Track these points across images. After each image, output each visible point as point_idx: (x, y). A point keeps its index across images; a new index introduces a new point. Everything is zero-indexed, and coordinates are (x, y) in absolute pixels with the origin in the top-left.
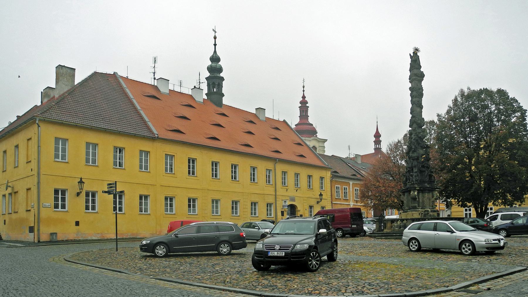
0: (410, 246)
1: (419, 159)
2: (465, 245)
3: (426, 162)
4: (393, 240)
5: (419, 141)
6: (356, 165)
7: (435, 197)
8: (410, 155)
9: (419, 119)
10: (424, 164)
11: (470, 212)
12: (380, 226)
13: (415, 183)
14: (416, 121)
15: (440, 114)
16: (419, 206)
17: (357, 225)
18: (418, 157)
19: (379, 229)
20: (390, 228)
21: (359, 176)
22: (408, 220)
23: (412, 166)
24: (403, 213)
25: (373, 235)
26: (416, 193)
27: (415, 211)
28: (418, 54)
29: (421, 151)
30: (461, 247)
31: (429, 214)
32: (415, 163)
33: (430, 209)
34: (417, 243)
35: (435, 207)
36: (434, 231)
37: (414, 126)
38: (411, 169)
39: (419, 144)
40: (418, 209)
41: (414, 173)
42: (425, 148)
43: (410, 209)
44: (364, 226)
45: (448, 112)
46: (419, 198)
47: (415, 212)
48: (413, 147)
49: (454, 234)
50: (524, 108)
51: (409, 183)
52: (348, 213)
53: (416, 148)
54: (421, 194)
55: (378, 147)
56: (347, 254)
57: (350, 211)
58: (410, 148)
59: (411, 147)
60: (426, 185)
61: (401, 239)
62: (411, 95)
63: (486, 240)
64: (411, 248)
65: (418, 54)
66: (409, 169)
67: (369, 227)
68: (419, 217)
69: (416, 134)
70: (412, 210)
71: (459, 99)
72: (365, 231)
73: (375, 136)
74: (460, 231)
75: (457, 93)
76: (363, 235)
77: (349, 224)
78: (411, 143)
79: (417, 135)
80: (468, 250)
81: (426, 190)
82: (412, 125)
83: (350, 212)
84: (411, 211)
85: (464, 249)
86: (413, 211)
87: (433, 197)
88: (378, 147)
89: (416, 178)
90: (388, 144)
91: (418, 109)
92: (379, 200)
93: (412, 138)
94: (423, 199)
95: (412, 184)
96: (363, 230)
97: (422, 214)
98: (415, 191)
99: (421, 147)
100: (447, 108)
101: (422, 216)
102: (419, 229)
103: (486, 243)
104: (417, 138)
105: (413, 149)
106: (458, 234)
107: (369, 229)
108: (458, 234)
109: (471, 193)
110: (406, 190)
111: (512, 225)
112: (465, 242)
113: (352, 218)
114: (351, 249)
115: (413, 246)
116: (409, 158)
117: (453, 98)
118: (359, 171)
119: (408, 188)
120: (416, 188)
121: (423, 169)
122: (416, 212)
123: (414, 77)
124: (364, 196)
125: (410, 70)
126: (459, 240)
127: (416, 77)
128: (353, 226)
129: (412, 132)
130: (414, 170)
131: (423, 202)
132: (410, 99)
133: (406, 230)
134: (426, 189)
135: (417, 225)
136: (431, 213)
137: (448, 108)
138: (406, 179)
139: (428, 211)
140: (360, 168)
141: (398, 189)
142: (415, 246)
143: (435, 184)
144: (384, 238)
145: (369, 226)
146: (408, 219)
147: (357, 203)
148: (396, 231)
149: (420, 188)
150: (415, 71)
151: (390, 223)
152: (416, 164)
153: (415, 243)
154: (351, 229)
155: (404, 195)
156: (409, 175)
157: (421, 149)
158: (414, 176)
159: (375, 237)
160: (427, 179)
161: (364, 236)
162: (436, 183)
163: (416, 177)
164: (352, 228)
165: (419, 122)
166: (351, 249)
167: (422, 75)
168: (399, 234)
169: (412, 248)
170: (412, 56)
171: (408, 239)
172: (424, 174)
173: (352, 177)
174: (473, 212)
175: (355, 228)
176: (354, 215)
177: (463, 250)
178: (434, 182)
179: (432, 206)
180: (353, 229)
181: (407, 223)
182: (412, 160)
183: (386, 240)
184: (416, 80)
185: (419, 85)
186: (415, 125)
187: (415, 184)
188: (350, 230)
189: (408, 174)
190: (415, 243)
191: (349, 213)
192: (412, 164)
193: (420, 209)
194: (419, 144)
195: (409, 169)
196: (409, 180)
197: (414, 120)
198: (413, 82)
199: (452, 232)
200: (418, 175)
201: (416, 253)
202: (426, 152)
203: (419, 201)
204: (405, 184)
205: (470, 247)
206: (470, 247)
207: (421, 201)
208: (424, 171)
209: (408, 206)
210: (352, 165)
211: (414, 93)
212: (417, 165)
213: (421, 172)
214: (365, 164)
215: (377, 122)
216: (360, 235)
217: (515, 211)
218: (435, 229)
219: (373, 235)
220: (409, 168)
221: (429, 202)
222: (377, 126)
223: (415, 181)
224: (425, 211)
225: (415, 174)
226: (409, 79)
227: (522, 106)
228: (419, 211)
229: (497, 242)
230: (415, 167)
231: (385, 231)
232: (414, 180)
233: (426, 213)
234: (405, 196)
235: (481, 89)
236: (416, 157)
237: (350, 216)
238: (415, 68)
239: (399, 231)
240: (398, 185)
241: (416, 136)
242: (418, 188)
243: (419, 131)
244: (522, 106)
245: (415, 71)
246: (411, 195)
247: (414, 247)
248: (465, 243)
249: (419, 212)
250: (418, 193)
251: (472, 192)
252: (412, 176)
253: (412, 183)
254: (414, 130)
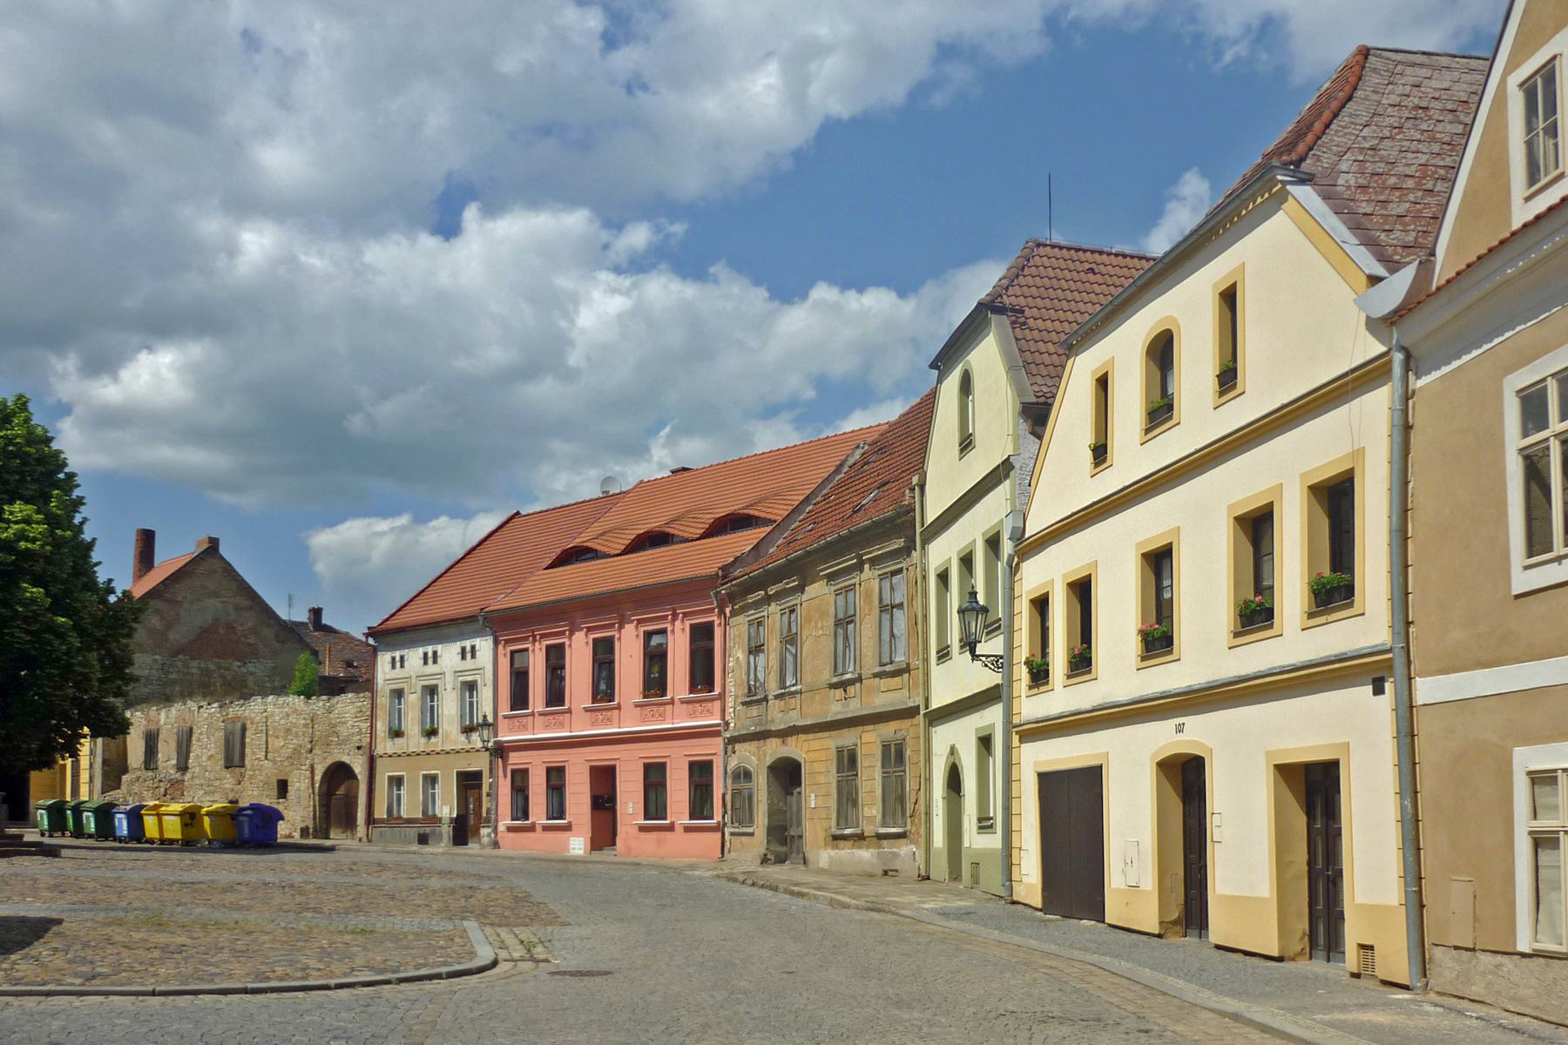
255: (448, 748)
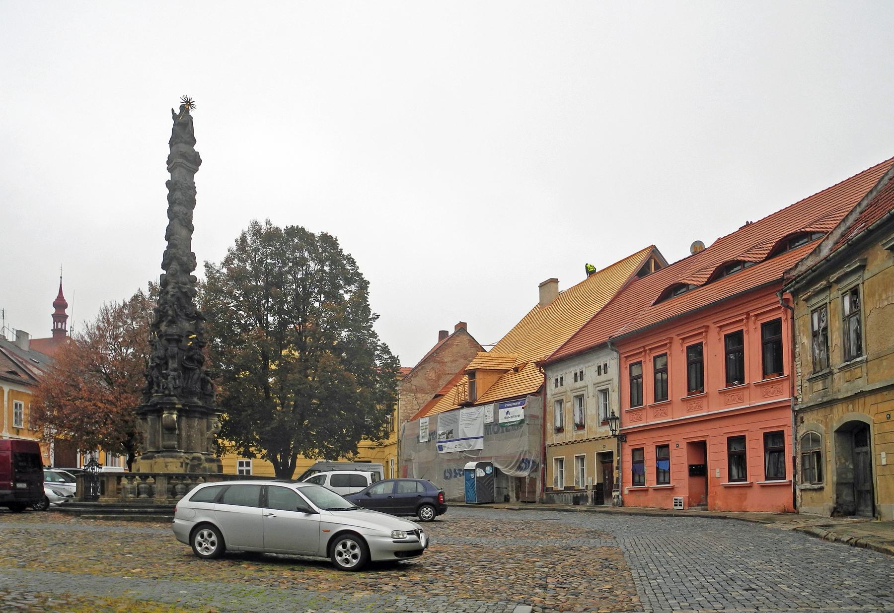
0: (196, 545)
1: (181, 341)
2: (344, 546)
3: (198, 351)
4: (125, 523)
5: (183, 301)
6: (17, 352)
7: (213, 429)
8: (161, 331)
9: (184, 252)
10: (192, 353)
11: (248, 468)
12: (87, 489)
13: (172, 393)
14: (178, 255)
15: (211, 262)
16: (179, 447)
17: (29, 483)
18: (179, 336)
19: (85, 495)
20: (116, 493)
21: (24, 377)
22: (157, 478)
23: (165, 356)
24: (142, 461)
25: (66, 508)
26: (175, 416)
27: (172, 457)
28: (191, 113)
29: (187, 325)
30: (331, 550)
31: (202, 467)
32: (173, 349)
33: (202, 454)
34: (214, 538)
35: (211, 452)
36: (260, 506)
37: (174, 266)
38: (163, 362)
39: (182, 307)
40: (178, 454)
41: (171, 371)
42: (193, 318)
43: (158, 452)
44: (45, 486)
45: (227, 262)
46: (180, 429)
47: (171, 460)
48: (170, 312)
49: (314, 517)
50: (366, 277)
51: (157, 392)
52: (7, 452)
53: (177, 315)
54: (184, 419)
55: (59, 327)
56: (24, 566)
57: (12, 448)
58: (161, 314)
59: (165, 311)
60: (196, 400)
61: (170, 520)
62: (169, 198)
63: (395, 533)
64: (199, 548)
65: (190, 111)
66: (158, 361)
67: (55, 490)
68: (181, 471)
69: (177, 286)
70: (164, 454)
71: (249, 239)
72: (46, 498)
73: (55, 305)
74: (327, 510)
75: (246, 226)
76: (42, 507)
77: (10, 480)
78: (166, 303)
79: (179, 288)
80: (350, 558)
81: (195, 411)
82: (169, 264)
83: (12, 451)
84: (163, 457)
85: (340, 554)
86: (167, 457)
87: (209, 428)
88: (59, 327)
89: (175, 383)
90: (103, 306)
91: (184, 232)
92: (78, 429)
93: (168, 292)
94: (188, 431)
95: (166, 396)
96: (44, 497)
97: (187, 464)
98: (172, 411)
99: (187, 315)
100: (226, 254)
101: (186, 468)
102: (220, 500)
103: (394, 542)
104: (179, 294)
105: (170, 318)
106: (324, 516)
107: (58, 493)
108: (324, 516)
109: (272, 428)
110: (151, 408)
111: (367, 497)
112: (344, 536)
113: (16, 465)
114: (30, 551)
115: (204, 545)
116: (160, 336)
117: (238, 236)
118: (27, 367)
119: (158, 403)
120: (175, 404)
121: (190, 365)
122: (175, 460)
123: (180, 160)
124: (39, 418)
125: (171, 143)
126: (329, 531)
127: (184, 161)
128: (19, 485)
129: (168, 279)
130: (170, 364)
131: (189, 437)
132: (167, 206)
133: (184, 503)
134: (194, 409)
135: (213, 491)
136: (207, 465)
137: (228, 253)
138: (151, 384)
139: (199, 459)
140: (28, 359)
141: (123, 409)
142: (209, 546)
143: (214, 401)
144: (103, 518)
145: (59, 488)
146: (159, 475)
147: (17, 435)
148: (130, 502)
149: (183, 405)
150: (183, 147)
151: (116, 482)
152: (176, 352)
153: (210, 535)
154: (14, 491)
155: (144, 419)
156: (158, 374)
157: (186, 319)
158: (169, 377)
159: (77, 514)
160: (197, 387)
161: (44, 510)
162: (215, 399)
163: (174, 379)
164: (15, 490)
165: (185, 259)
166: (30, 551)
167: (196, 161)
168: (136, 507)
169: (202, 550)
170: (178, 114)
171: (192, 524)
172: (191, 375)
173: (10, 377)
174: (253, 469)
175: (23, 489)
176: (20, 459)
177: (338, 558)
178: (212, 396)
179: (207, 448)
180: (18, 492)
181: (155, 483)
182: (164, 342)
183: (108, 523)
184: (183, 167)
185: (188, 179)
186: (177, 264)
187: (173, 396)
188: (12, 493)
189: (155, 373)
190: (210, 535)
191: (9, 453)
192: (166, 350)
193: (182, 454)
194: (182, 307)
195: (158, 361)
196: (158, 386)
197: (174, 253)
198: (177, 172)
199: (309, 511)
200: (179, 377)
201: (215, 564)
202: (196, 329)
203: (180, 435)
204: (147, 393)
205: (357, 551)
206: (357, 551)
207: (184, 435)
208: (192, 370)
209: (153, 443)
210: (10, 352)
211: (178, 195)
212: (177, 353)
213: (186, 370)
214: (37, 353)
215: (61, 278)
216: (33, 508)
217: (356, 470)
218: (263, 502)
219: (66, 508)
220: (158, 357)
221: (202, 439)
222: (61, 285)
223: (172, 389)
224: (194, 458)
225: (172, 373)
226: (168, 163)
227: (362, 274)
228: (181, 457)
229: (414, 537)
230: (173, 357)
231: (103, 500)
232: (171, 386)
233: (196, 462)
234: (147, 423)
235: (292, 226)
236: (177, 335)
237: (11, 461)
238: (183, 141)
239: (137, 502)
240: (122, 399)
241: (176, 290)
242: (180, 406)
243: (184, 279)
244: (362, 274)
245: (183, 147)
246: (163, 420)
247: (207, 548)
248: (200, 532)
249: (182, 460)
250: (179, 417)
251: (273, 426)
252: (166, 377)
253: (167, 392)
254: (173, 275)
255: (591, 437)
